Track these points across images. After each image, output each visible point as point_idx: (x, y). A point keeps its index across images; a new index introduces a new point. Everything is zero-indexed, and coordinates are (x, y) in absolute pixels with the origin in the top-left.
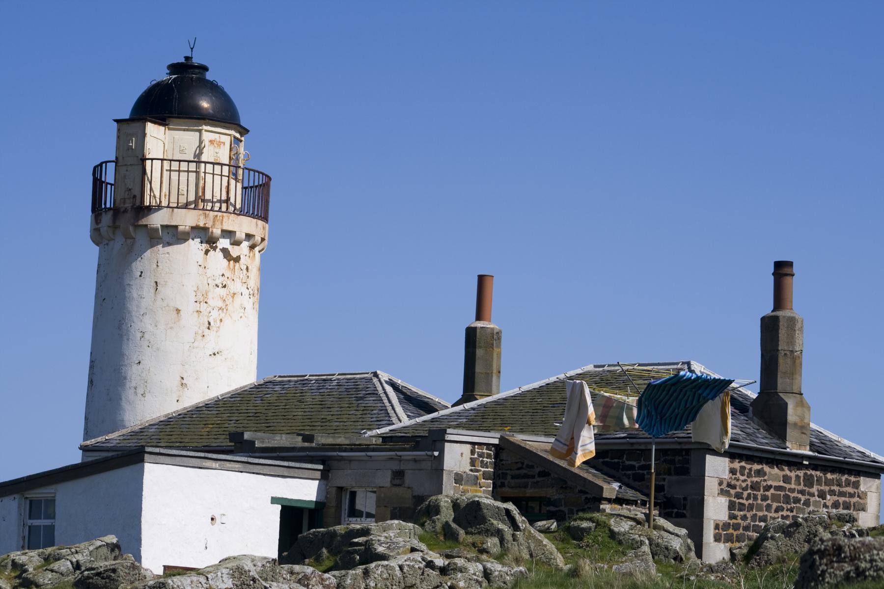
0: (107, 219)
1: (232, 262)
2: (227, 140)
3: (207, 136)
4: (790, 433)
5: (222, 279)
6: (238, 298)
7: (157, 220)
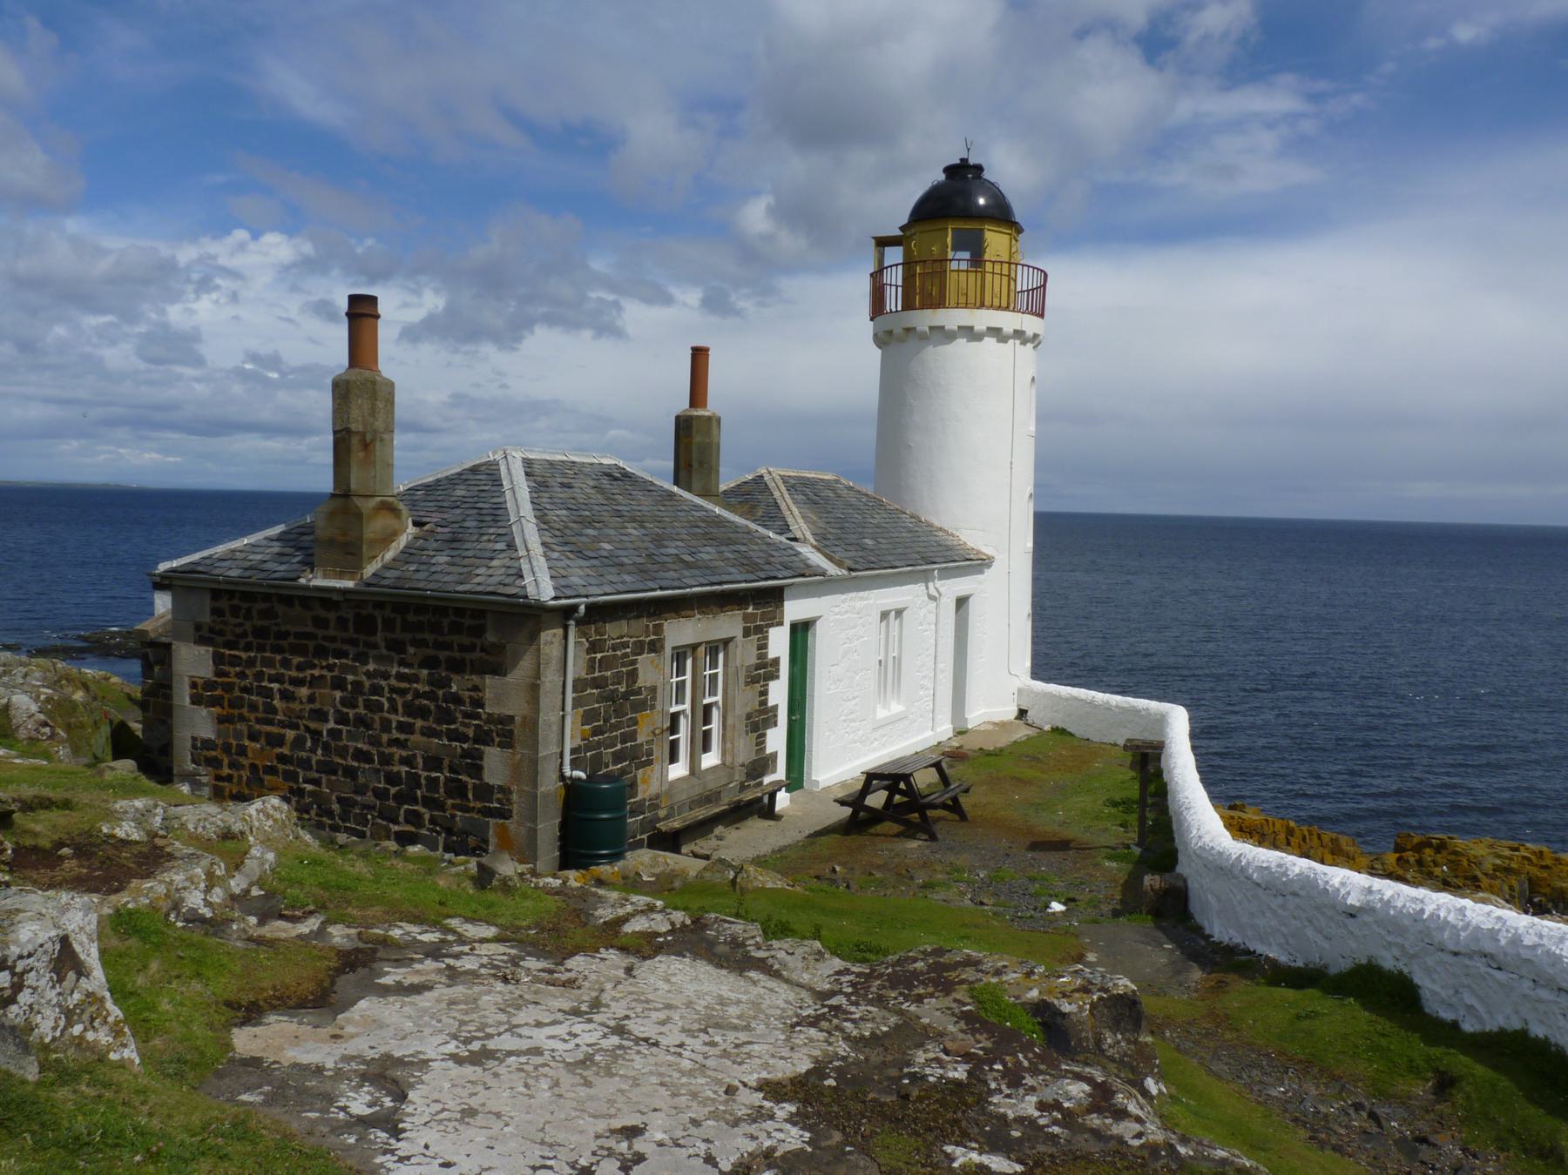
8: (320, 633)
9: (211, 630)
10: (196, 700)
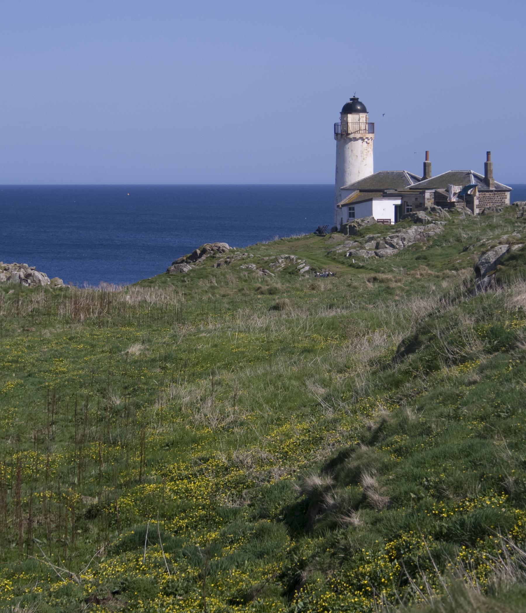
0: (339, 136)
2: (365, 116)
3: (361, 116)
4: (491, 185)
7: (351, 136)
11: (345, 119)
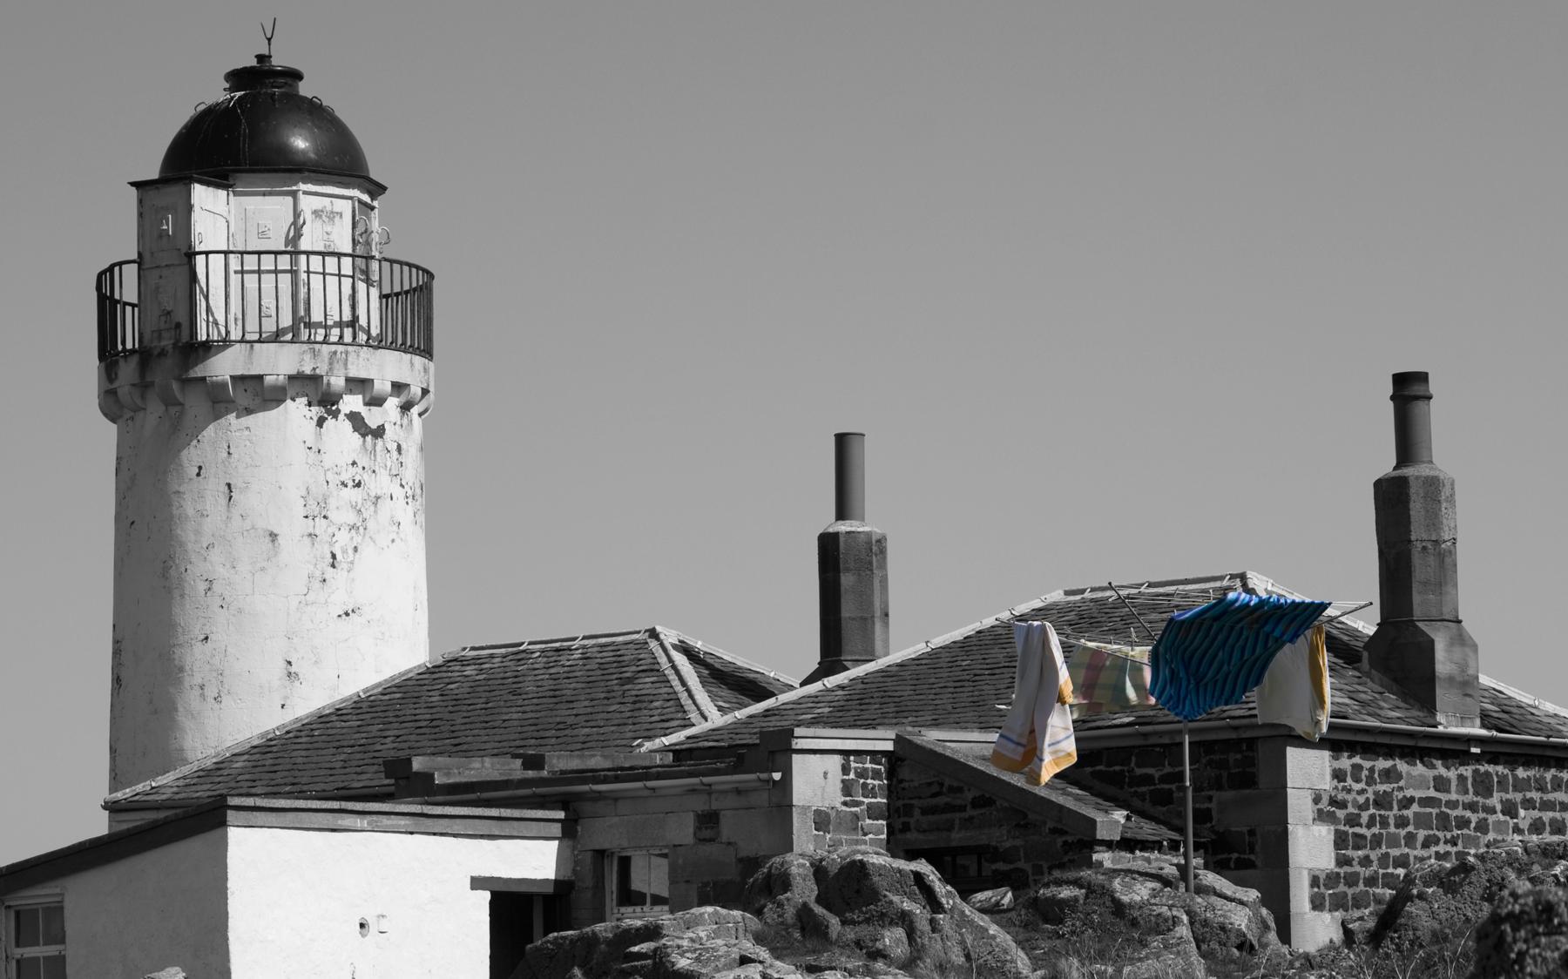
1: (369, 438)
2: (345, 207)
3: (308, 204)
4: (1443, 695)
5: (355, 469)
6: (385, 505)
7: (223, 367)
8: (1443, 797)
9: (1333, 802)
10: (1317, 904)
11: (168, 226)
